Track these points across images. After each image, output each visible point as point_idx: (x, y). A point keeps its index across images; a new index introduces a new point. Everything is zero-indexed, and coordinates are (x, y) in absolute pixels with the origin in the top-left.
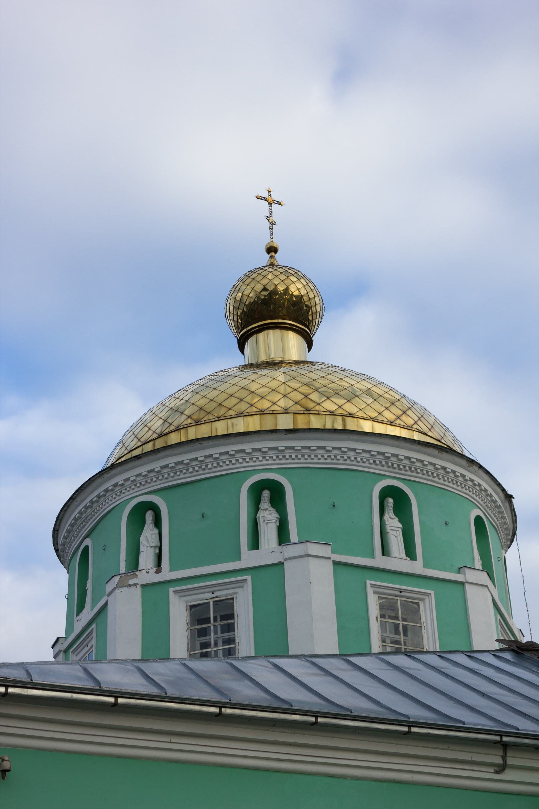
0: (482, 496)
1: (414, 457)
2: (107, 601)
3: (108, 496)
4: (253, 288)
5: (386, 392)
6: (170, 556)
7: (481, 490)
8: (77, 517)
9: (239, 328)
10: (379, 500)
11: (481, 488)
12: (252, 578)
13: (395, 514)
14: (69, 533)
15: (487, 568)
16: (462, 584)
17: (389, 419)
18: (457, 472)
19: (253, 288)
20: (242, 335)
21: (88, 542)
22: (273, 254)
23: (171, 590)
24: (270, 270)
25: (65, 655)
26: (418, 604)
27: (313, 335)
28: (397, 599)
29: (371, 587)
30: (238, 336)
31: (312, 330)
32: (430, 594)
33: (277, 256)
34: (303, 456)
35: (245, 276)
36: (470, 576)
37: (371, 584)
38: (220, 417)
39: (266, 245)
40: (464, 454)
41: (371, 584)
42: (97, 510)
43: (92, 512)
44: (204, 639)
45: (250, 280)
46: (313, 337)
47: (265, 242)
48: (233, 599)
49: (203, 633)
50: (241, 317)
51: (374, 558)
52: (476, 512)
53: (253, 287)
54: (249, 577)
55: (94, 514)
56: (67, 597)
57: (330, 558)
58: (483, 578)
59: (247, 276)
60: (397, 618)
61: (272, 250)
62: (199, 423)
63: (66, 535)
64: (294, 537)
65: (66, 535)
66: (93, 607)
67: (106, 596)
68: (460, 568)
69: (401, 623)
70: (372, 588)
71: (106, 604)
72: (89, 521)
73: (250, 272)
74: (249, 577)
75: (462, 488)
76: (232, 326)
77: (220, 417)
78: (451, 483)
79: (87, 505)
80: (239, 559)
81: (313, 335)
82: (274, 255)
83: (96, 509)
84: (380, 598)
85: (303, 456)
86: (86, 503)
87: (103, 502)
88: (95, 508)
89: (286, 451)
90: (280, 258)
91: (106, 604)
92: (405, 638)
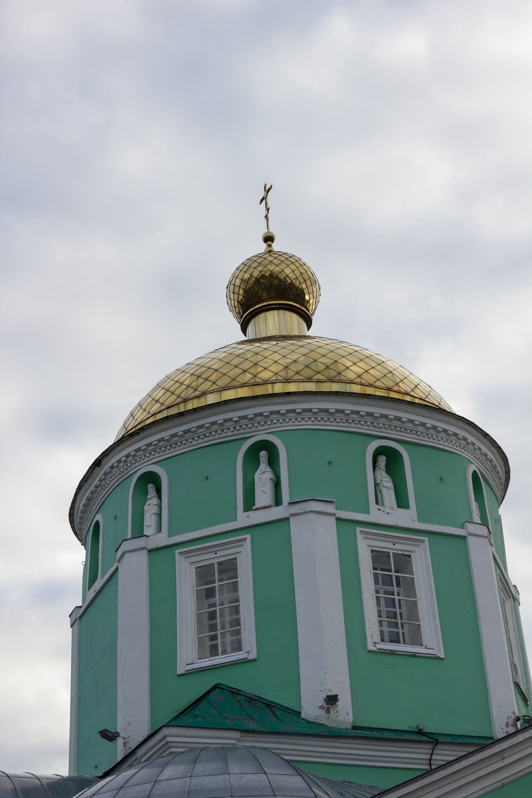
0: (467, 449)
1: (207, 422)
2: (118, 566)
3: (120, 467)
4: (251, 275)
5: (379, 364)
6: (149, 437)
7: (467, 444)
8: (107, 472)
9: (239, 315)
10: (404, 465)
11: (467, 441)
12: (251, 536)
13: (387, 472)
14: (90, 500)
15: (484, 522)
16: (464, 538)
17: (403, 384)
18: (449, 430)
19: (251, 275)
20: (245, 316)
21: (99, 517)
22: (270, 243)
23: (177, 552)
24: (270, 259)
25: (80, 621)
26: (409, 556)
27: (311, 314)
28: (389, 552)
29: (361, 533)
30: (241, 321)
31: (310, 310)
32: (424, 541)
33: (273, 245)
34: (272, 421)
35: (243, 266)
36: (472, 528)
37: (360, 531)
38: (288, 379)
39: (263, 235)
40: (452, 412)
41: (360, 531)
42: (113, 478)
43: (105, 484)
44: (211, 601)
45: (246, 268)
46: (312, 317)
47: (264, 231)
48: (235, 559)
49: (210, 593)
50: (241, 302)
51: (369, 514)
52: (472, 468)
53: (251, 274)
54: (248, 537)
55: (105, 488)
56: (84, 563)
57: (334, 515)
58: (483, 531)
59: (246, 265)
60: (390, 571)
61: (269, 239)
62: (288, 381)
63: (82, 509)
64: (286, 498)
65: (82, 509)
66: (102, 578)
67: (117, 563)
68: (463, 523)
69: (394, 574)
70: (363, 535)
71: (117, 569)
72: (87, 522)
73: (178, 371)
74: (248, 537)
75: (453, 445)
76: (235, 306)
77: (288, 379)
78: (431, 438)
79: (102, 478)
80: (235, 519)
81: (311, 314)
82: (270, 244)
83: (117, 472)
84: (372, 551)
85: (353, 421)
86: (92, 489)
87: (121, 469)
88: (115, 472)
89: (337, 415)
90: (276, 246)
91: (117, 569)
92: (399, 589)
